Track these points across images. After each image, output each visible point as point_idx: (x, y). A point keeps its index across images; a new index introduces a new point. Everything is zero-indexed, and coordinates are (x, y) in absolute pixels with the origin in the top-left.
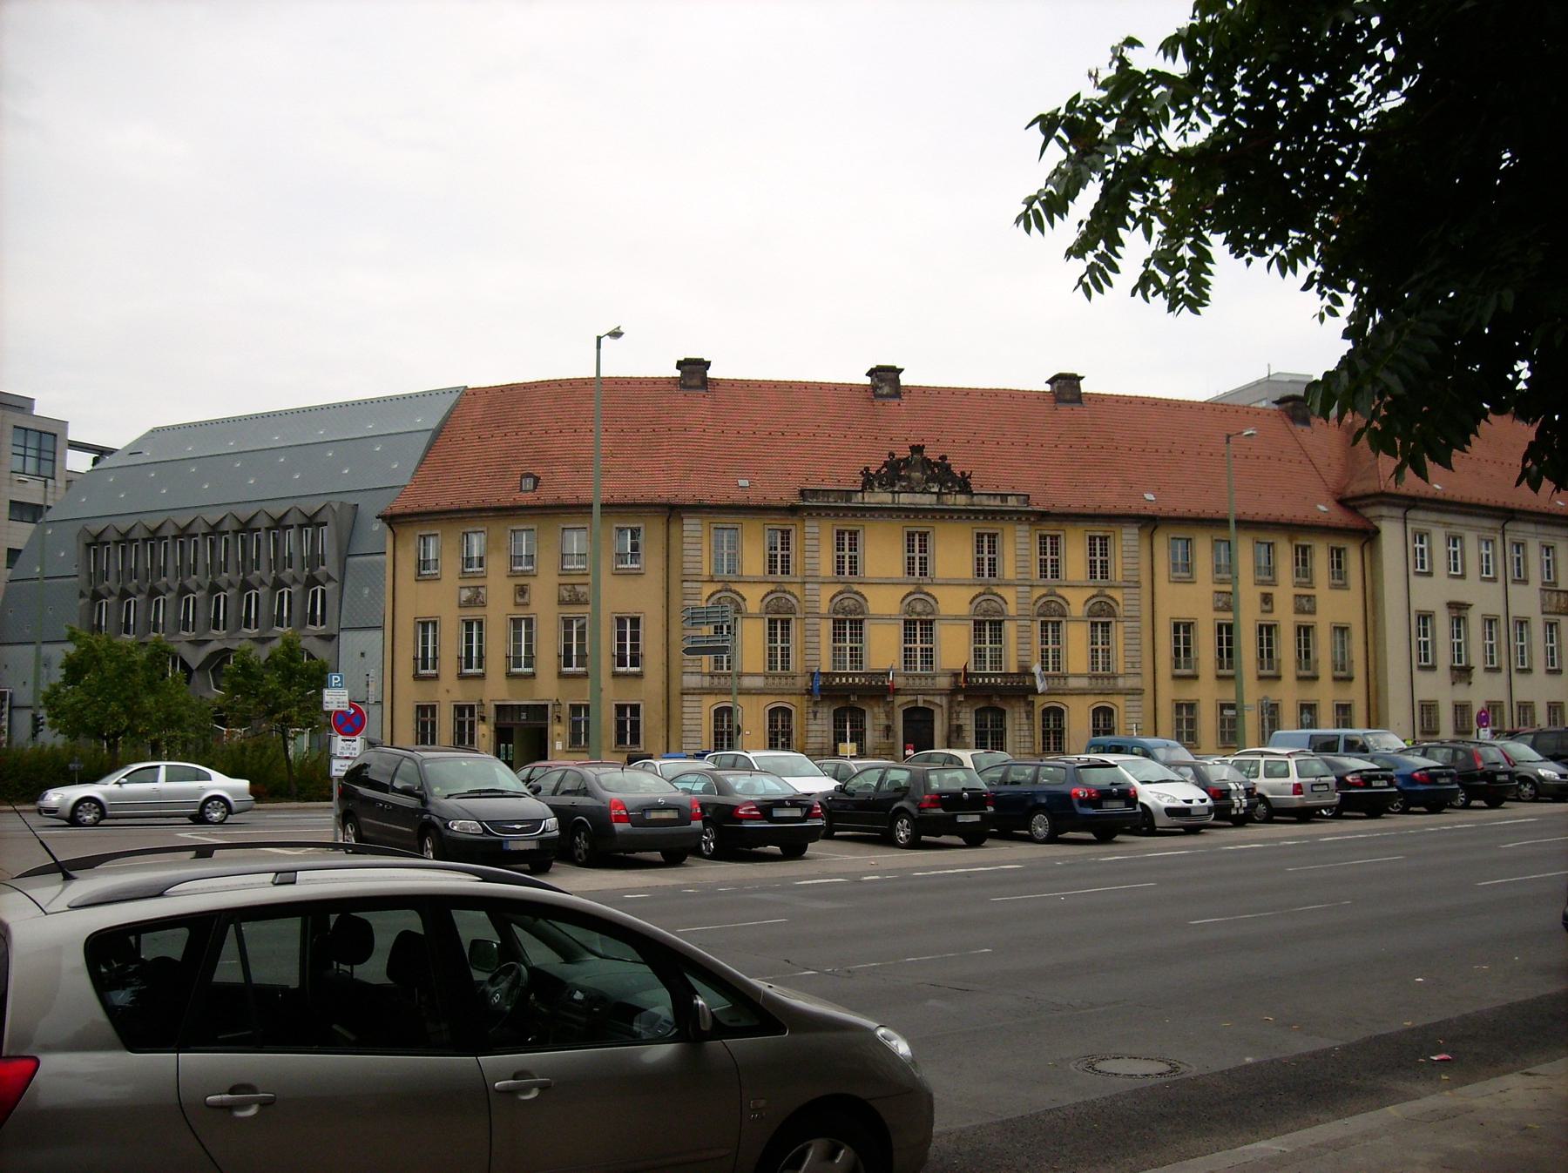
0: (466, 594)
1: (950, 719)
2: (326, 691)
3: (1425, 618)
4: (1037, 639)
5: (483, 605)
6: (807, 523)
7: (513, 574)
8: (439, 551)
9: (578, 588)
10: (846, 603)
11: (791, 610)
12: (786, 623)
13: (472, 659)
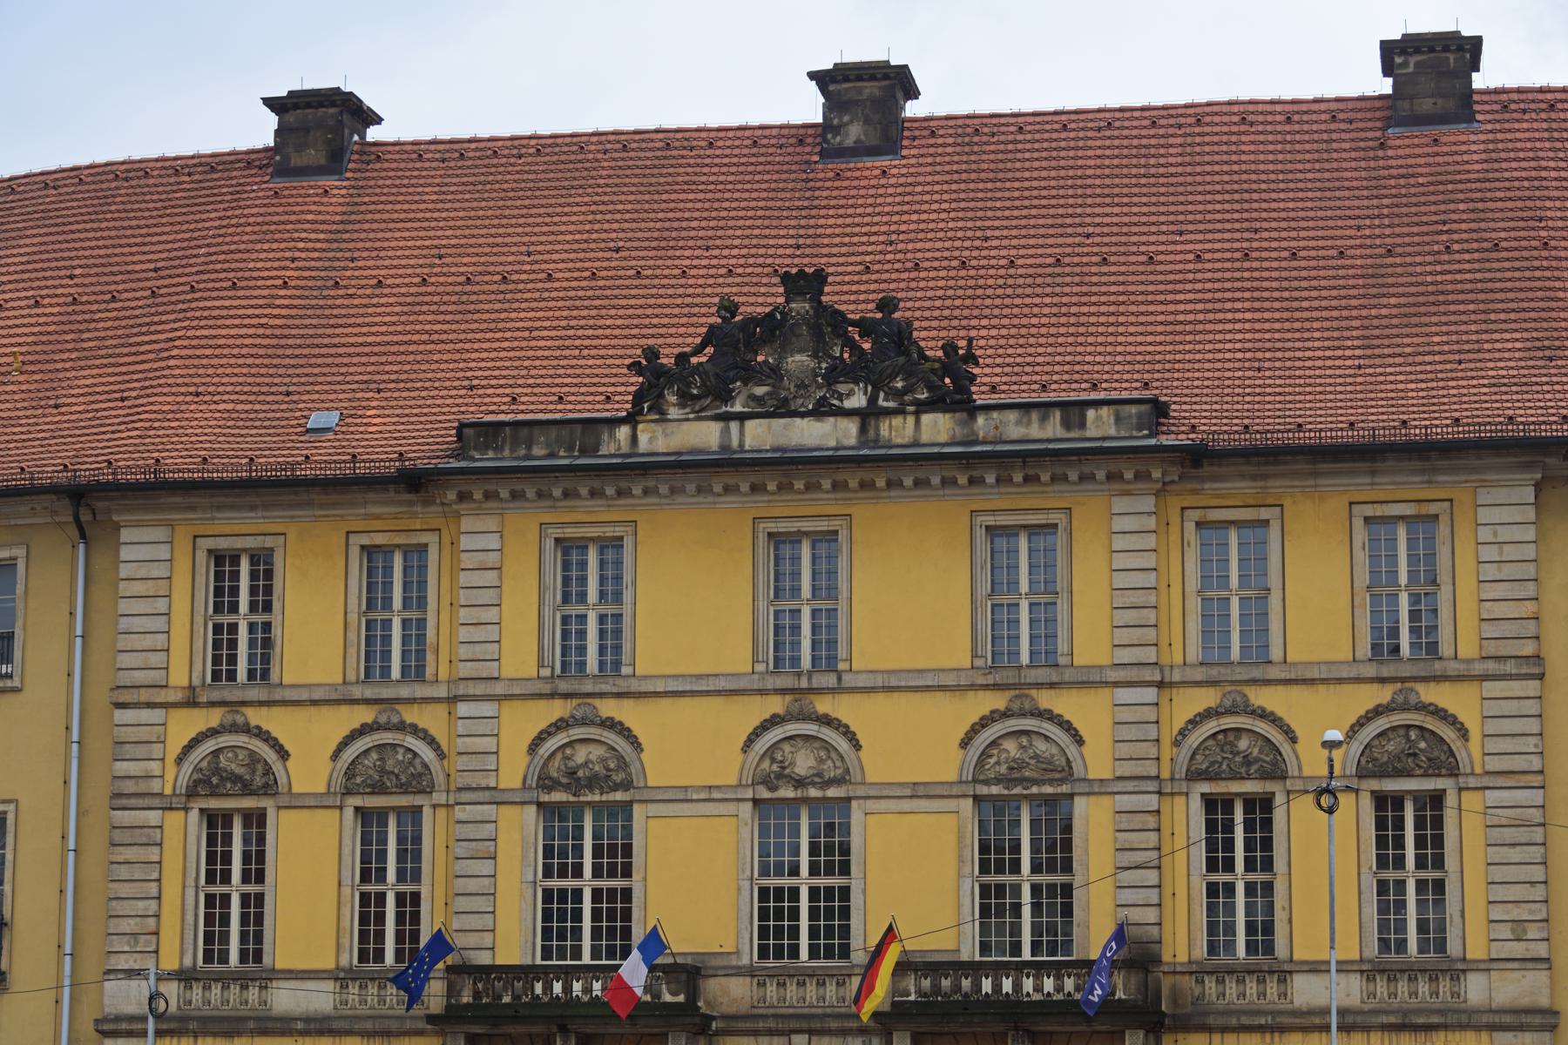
2: (1141, 1033)
6: (467, 523)
10: (581, 755)
11: (418, 781)
12: (1260, 808)
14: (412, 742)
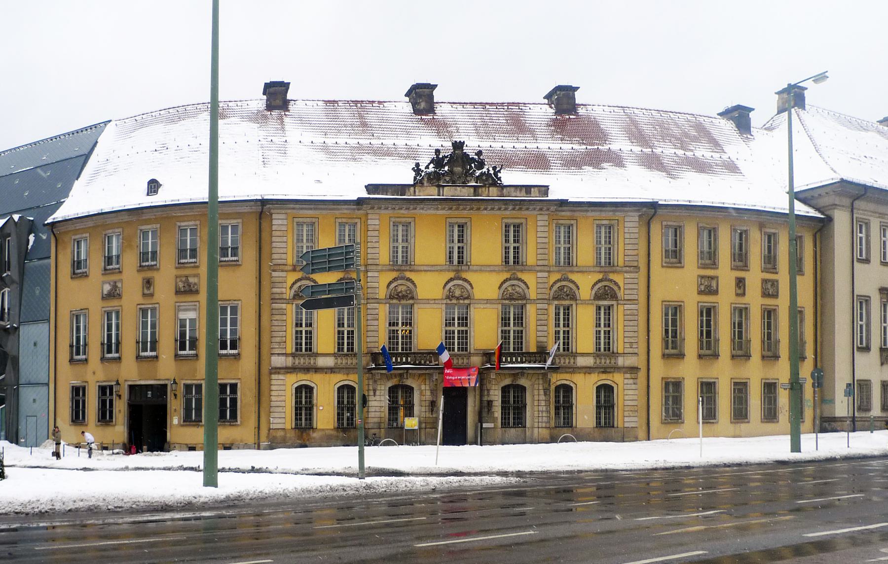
0: (107, 288)
1: (481, 396)
3: (865, 301)
4: (552, 322)
5: (119, 296)
7: (141, 268)
8: (88, 253)
9: (191, 280)
13: (111, 346)
14: (571, 285)
